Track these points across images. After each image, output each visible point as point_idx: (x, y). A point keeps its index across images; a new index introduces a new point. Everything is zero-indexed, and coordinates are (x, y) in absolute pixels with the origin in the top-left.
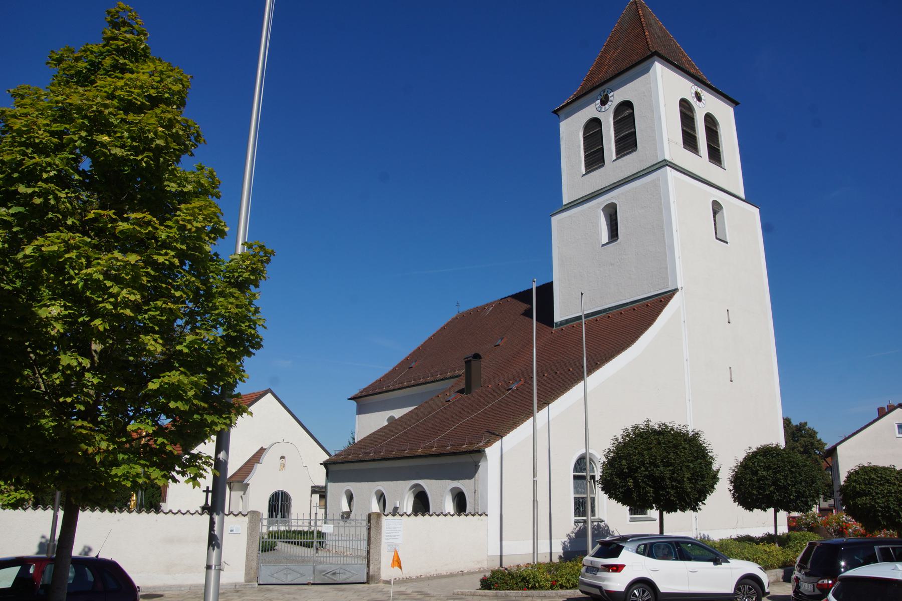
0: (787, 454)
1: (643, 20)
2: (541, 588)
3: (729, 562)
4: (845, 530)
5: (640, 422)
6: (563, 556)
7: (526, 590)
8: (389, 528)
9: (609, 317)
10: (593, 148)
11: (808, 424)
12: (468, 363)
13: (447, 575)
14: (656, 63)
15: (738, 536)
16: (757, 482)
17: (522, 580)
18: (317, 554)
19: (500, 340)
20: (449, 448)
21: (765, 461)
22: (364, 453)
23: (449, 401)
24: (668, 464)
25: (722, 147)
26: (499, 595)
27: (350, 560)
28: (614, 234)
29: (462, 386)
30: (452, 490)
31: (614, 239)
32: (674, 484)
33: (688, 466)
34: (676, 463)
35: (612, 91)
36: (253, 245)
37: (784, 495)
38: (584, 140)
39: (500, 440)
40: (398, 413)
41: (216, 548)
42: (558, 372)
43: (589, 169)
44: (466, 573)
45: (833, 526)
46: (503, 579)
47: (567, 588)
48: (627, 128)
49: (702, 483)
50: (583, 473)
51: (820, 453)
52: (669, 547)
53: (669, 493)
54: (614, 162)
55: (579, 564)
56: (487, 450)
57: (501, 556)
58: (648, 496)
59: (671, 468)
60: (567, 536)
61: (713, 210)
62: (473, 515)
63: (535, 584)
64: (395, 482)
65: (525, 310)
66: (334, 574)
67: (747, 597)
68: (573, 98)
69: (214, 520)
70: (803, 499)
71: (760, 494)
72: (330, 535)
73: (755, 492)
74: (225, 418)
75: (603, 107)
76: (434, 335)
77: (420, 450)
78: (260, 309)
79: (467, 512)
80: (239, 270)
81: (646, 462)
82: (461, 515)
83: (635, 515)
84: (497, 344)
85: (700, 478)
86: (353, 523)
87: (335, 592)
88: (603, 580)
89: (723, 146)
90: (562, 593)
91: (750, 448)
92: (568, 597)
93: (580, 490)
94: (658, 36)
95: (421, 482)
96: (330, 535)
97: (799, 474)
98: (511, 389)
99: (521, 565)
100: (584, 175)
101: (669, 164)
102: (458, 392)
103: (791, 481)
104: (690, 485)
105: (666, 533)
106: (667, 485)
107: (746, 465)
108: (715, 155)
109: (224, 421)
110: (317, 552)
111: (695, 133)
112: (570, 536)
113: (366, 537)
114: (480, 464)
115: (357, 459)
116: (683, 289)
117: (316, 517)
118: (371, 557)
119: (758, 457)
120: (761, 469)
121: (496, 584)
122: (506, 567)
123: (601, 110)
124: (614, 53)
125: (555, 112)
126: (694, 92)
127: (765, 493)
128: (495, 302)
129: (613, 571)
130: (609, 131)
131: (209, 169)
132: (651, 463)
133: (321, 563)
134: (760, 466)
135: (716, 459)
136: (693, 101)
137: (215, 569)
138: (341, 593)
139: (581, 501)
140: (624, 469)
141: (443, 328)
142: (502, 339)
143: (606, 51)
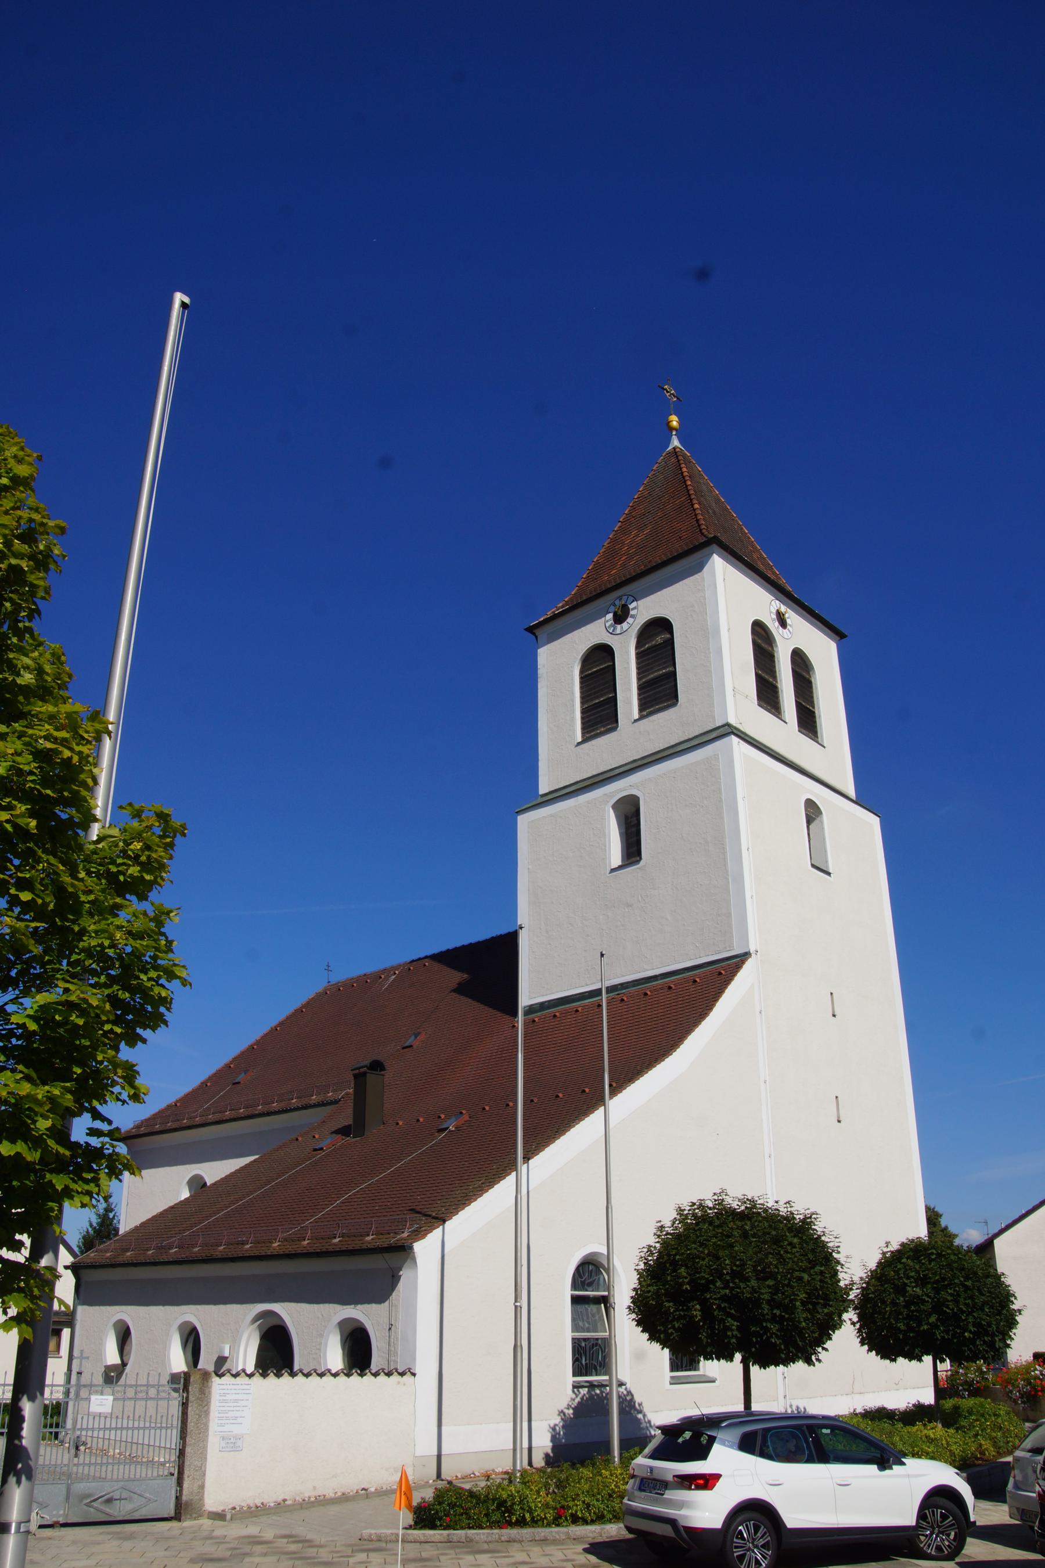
0: (955, 1254)
1: (689, 483)
2: (535, 1522)
3: (903, 1464)
4: (1040, 1394)
5: (706, 1194)
6: (551, 1455)
7: (507, 1528)
8: (225, 1401)
9: (622, 1000)
10: (598, 697)
12: (360, 1078)
13: (335, 1499)
14: (715, 556)
16: (905, 1307)
17: (498, 1508)
18: (76, 1459)
19: (413, 1037)
20: (337, 1240)
21: (917, 1267)
22: (158, 1248)
23: (322, 1149)
24: (764, 1275)
25: (819, 708)
26: (455, 1539)
27: (138, 1470)
28: (632, 850)
29: (346, 1118)
30: (342, 1324)
31: (634, 859)
32: (777, 1312)
33: (800, 1279)
34: (778, 1273)
35: (635, 599)
36: (143, 811)
37: (953, 1330)
38: (581, 683)
39: (441, 1227)
40: (214, 1171)
41: (24, 1478)
42: (536, 1100)
43: (588, 732)
44: (373, 1493)
45: (1018, 1387)
46: (461, 1506)
47: (585, 1522)
48: (659, 665)
49: (826, 1311)
50: (587, 1291)
52: (795, 1436)
53: (767, 1329)
54: (635, 724)
55: (603, 1471)
56: (418, 1247)
57: (439, 1457)
58: (728, 1337)
59: (770, 1282)
60: (559, 1415)
61: (807, 815)
62: (389, 1374)
63: (524, 1515)
64: (221, 1307)
65: (459, 984)
66: (109, 1501)
67: (940, 1532)
68: (563, 607)
69: (23, 1413)
70: (986, 1338)
71: (910, 1329)
72: (106, 1417)
73: (901, 1326)
74: (87, 1181)
75: (619, 627)
76: (281, 1024)
77: (276, 1245)
78: (175, 943)
79: (374, 1366)
80: (119, 861)
81: (725, 1271)
82: (365, 1375)
83: (678, 1371)
84: (407, 1044)
85: (822, 1301)
86: (130, 1392)
87: (116, 1543)
88: (681, 1505)
90: (578, 1533)
91: (887, 1244)
92: (591, 1540)
93: (581, 1324)
94: (714, 512)
95: (277, 1307)
96: (106, 1417)
97: (979, 1290)
98: (446, 1129)
99: (477, 1474)
100: (579, 744)
101: (735, 731)
102: (337, 1132)
103: (965, 1304)
104: (804, 1316)
105: (755, 1407)
106: (763, 1315)
107: (882, 1275)
108: (808, 721)
109: (86, 1187)
110: (76, 1456)
111: (777, 682)
112: (564, 1414)
113: (176, 1422)
114: (401, 1273)
115: (142, 1259)
116: (758, 954)
117: (78, 1379)
118: (187, 1463)
119: (904, 1260)
120: (911, 1282)
121: (445, 1515)
122: (449, 1479)
123: (613, 631)
124: (637, 536)
125: (531, 630)
126: (775, 612)
127: (922, 1329)
128: (400, 965)
129: (699, 1487)
130: (628, 669)
131: (53, 646)
132: (734, 1274)
133: (86, 1478)
134: (908, 1278)
135: (847, 1265)
136: (773, 626)
137: (18, 1530)
138: (127, 1545)
139: (583, 1344)
140: (683, 1284)
141: (299, 1011)
142: (416, 1035)
143: (624, 531)
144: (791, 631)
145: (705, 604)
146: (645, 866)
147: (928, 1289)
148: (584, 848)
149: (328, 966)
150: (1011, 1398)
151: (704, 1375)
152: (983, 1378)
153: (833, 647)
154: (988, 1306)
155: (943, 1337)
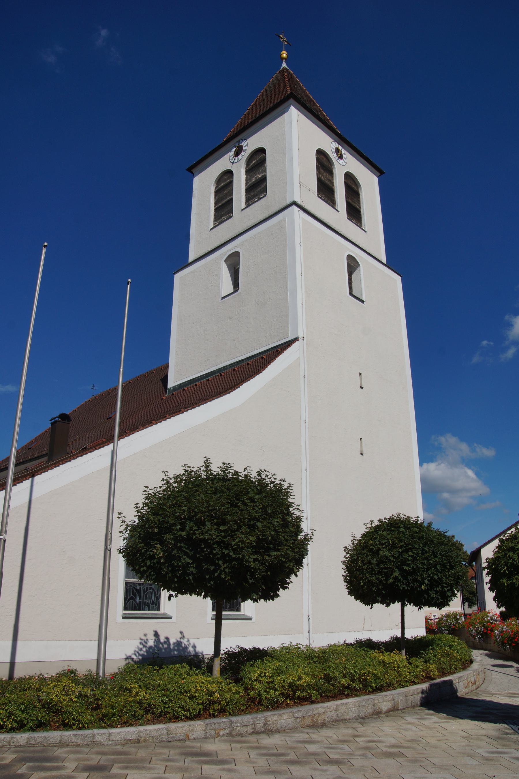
11: (455, 537)
14: (292, 108)
15: (357, 641)
51: (465, 564)
89: (364, 198)
91: (371, 522)
120: (383, 548)
136: (333, 156)
139: (138, 587)
144: (346, 161)
145: (285, 135)
146: (240, 293)
147: (395, 552)
148: (208, 288)
149: (93, 387)
150: (472, 635)
151: (243, 615)
152: (457, 622)
153: (375, 180)
154: (439, 565)
155: (404, 588)
